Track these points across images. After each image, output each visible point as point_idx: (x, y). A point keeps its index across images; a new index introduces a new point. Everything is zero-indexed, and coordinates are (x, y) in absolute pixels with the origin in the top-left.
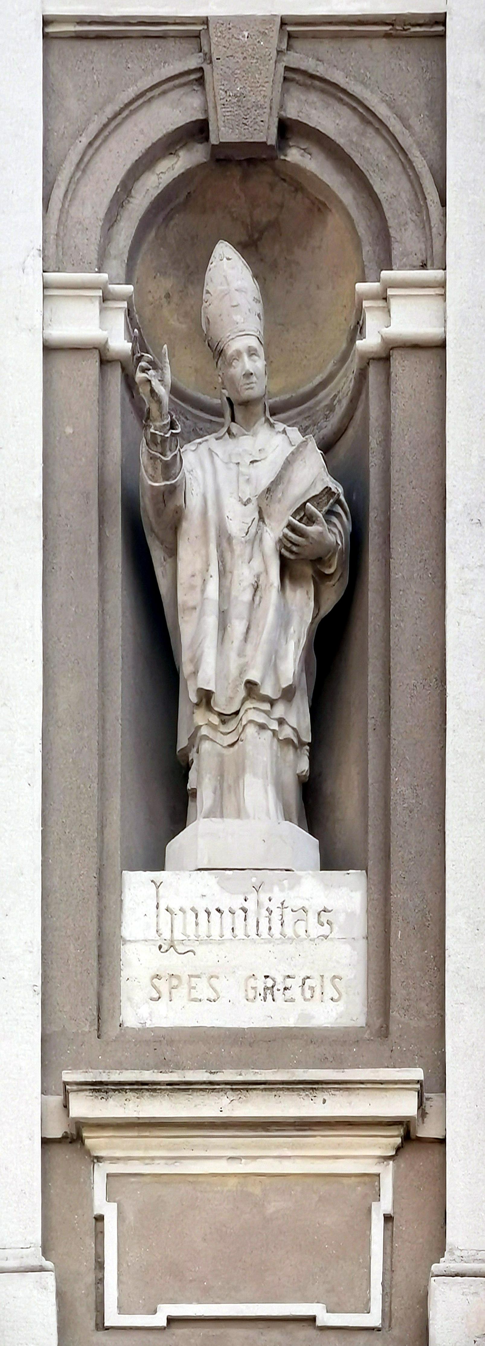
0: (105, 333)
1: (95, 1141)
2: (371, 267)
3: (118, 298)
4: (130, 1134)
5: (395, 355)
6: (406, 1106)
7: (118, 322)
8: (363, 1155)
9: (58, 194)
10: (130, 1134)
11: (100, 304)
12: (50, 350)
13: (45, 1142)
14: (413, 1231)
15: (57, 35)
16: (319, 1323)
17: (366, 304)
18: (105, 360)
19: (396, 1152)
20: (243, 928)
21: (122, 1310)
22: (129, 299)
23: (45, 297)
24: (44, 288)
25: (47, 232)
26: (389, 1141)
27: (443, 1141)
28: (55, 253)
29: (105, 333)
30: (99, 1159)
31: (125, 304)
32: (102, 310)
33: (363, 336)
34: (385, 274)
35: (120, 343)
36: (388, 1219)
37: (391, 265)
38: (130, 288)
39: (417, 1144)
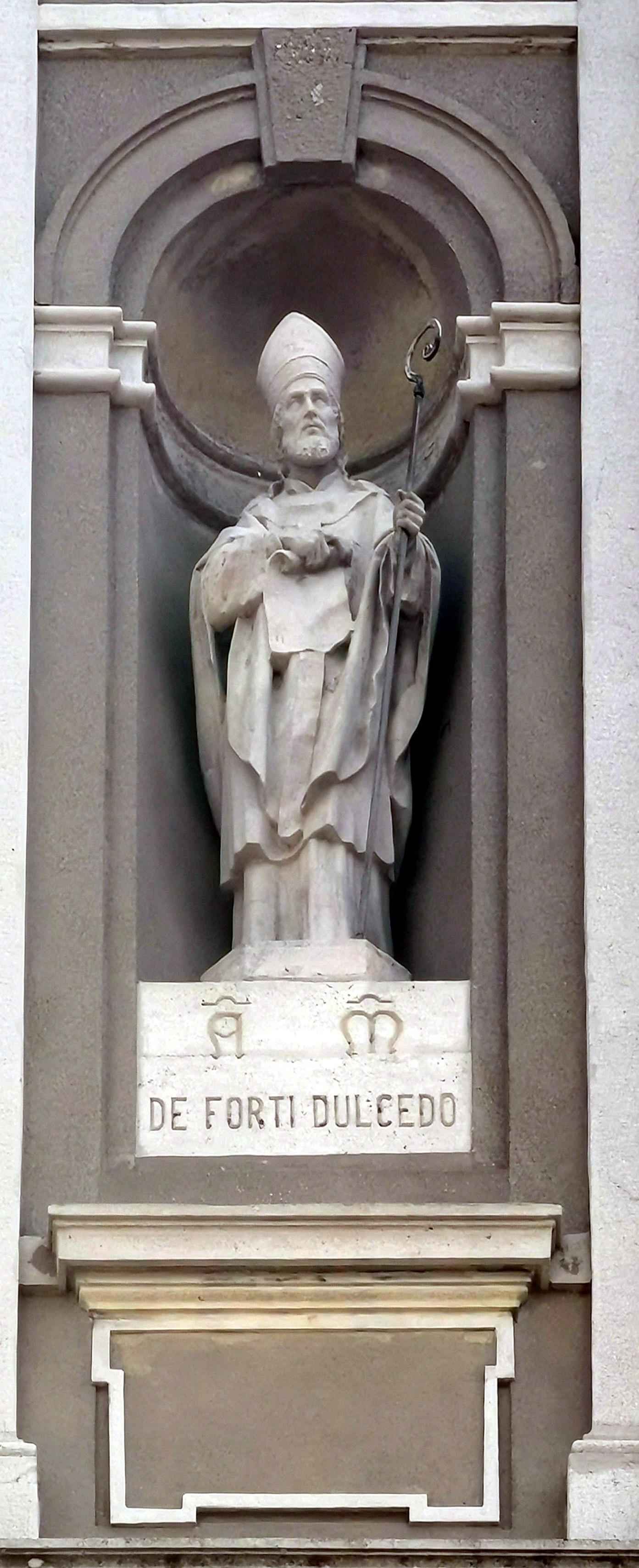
0: (116, 372)
1: (91, 1292)
2: (476, 301)
3: (135, 335)
4: (127, 1282)
5: (512, 402)
6: (535, 1247)
7: (136, 364)
8: (491, 1316)
9: (56, 221)
10: (127, 1282)
11: (111, 341)
12: (44, 391)
13: (26, 1293)
14: (541, 1403)
15: (56, 56)
16: (413, 1518)
17: (469, 340)
18: (118, 404)
19: (521, 1306)
20: (313, 1047)
21: (131, 1502)
22: (148, 336)
23: (36, 332)
24: (35, 324)
25: (583, 1188)
26: (511, 1291)
27: (586, 1290)
28: (49, 286)
29: (116, 372)
30: (103, 1314)
31: (145, 344)
32: (113, 350)
33: (466, 375)
34: (496, 305)
35: (134, 381)
36: (503, 1384)
37: (503, 296)
38: (152, 325)
39: (554, 1295)
